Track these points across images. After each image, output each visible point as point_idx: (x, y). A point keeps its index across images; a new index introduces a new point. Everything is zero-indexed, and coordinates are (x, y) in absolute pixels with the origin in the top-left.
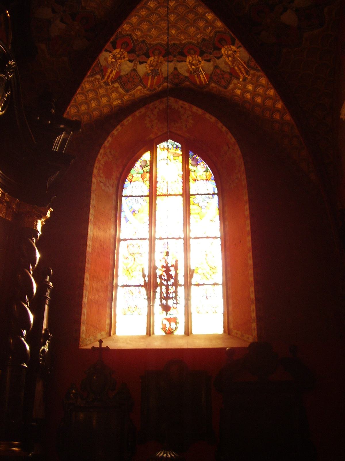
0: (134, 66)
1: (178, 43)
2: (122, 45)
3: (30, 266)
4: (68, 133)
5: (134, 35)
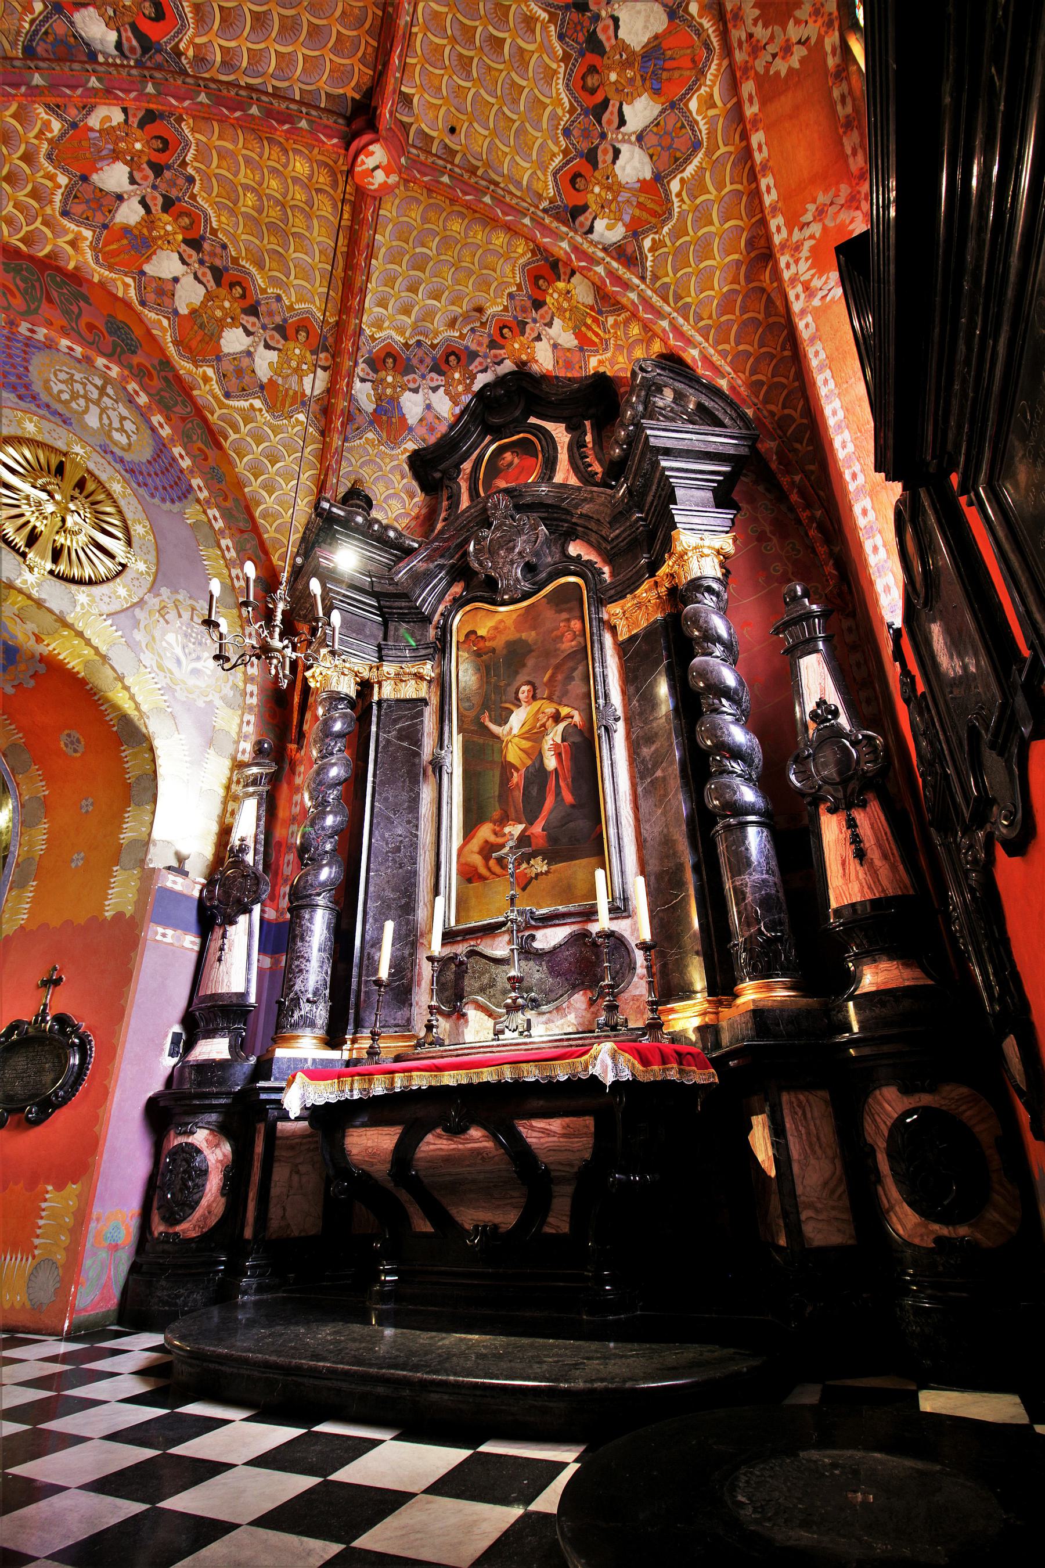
0: (629, 142)
1: (552, 28)
2: (578, 190)
3: (143, 1501)
4: (331, 868)
5: (554, 165)
